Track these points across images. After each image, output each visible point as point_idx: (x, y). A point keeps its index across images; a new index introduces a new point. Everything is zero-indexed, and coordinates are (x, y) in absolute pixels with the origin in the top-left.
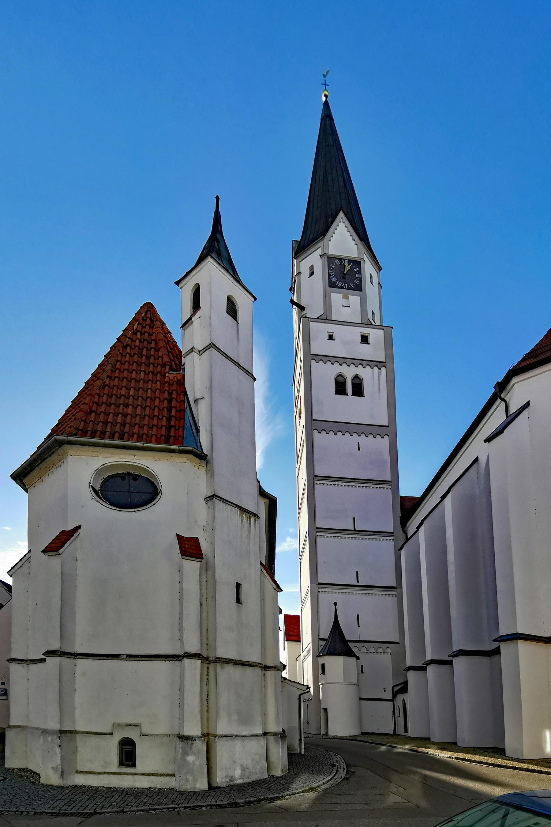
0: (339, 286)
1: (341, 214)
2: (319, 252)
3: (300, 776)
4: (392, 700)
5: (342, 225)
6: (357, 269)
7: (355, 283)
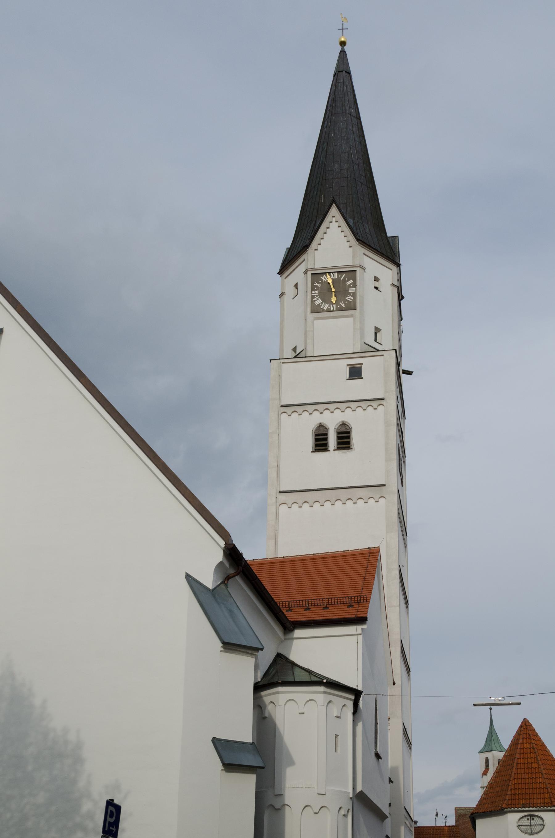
0: (325, 308)
1: (334, 211)
2: (302, 268)
3: (449, 829)
4: (516, 753)
5: (334, 226)
6: (351, 281)
7: (347, 300)
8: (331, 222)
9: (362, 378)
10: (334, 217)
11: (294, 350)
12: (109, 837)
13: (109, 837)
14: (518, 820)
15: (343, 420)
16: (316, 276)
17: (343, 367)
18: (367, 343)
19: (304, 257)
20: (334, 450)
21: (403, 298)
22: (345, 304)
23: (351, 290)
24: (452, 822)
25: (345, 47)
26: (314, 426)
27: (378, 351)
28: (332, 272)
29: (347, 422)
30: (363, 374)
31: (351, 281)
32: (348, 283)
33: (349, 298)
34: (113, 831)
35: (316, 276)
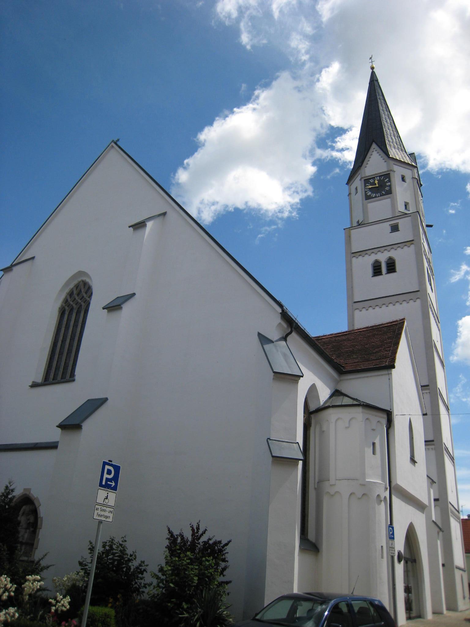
0: (374, 196)
2: (359, 178)
6: (387, 179)
8: (373, 152)
9: (399, 231)
10: (374, 149)
11: (358, 222)
12: (439, 542)
13: (439, 542)
14: (308, 610)
15: (390, 256)
16: (367, 181)
17: (387, 226)
18: (400, 211)
19: (360, 172)
20: (386, 274)
21: (421, 185)
22: (385, 192)
23: (388, 184)
24: (233, 210)
25: (374, 70)
26: (372, 261)
27: (406, 214)
28: (376, 177)
29: (391, 257)
30: (400, 229)
31: (387, 179)
32: (386, 181)
33: (387, 188)
34: (112, 485)
35: (367, 181)
